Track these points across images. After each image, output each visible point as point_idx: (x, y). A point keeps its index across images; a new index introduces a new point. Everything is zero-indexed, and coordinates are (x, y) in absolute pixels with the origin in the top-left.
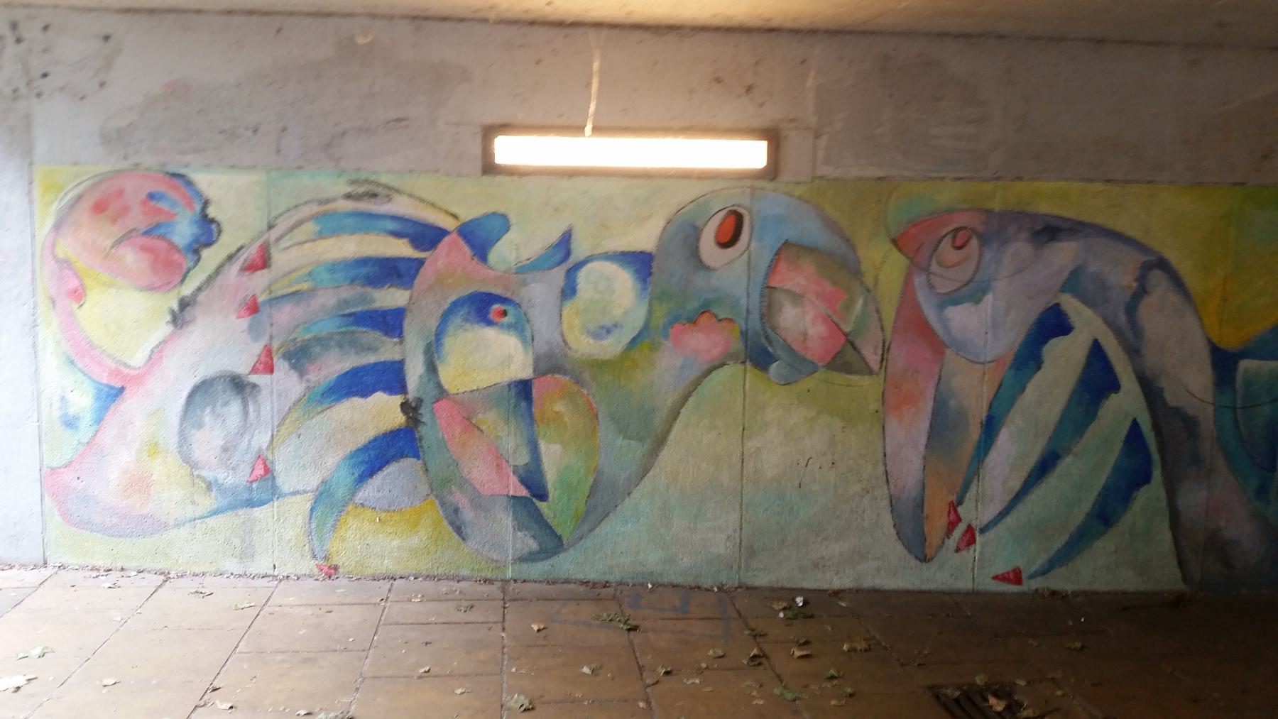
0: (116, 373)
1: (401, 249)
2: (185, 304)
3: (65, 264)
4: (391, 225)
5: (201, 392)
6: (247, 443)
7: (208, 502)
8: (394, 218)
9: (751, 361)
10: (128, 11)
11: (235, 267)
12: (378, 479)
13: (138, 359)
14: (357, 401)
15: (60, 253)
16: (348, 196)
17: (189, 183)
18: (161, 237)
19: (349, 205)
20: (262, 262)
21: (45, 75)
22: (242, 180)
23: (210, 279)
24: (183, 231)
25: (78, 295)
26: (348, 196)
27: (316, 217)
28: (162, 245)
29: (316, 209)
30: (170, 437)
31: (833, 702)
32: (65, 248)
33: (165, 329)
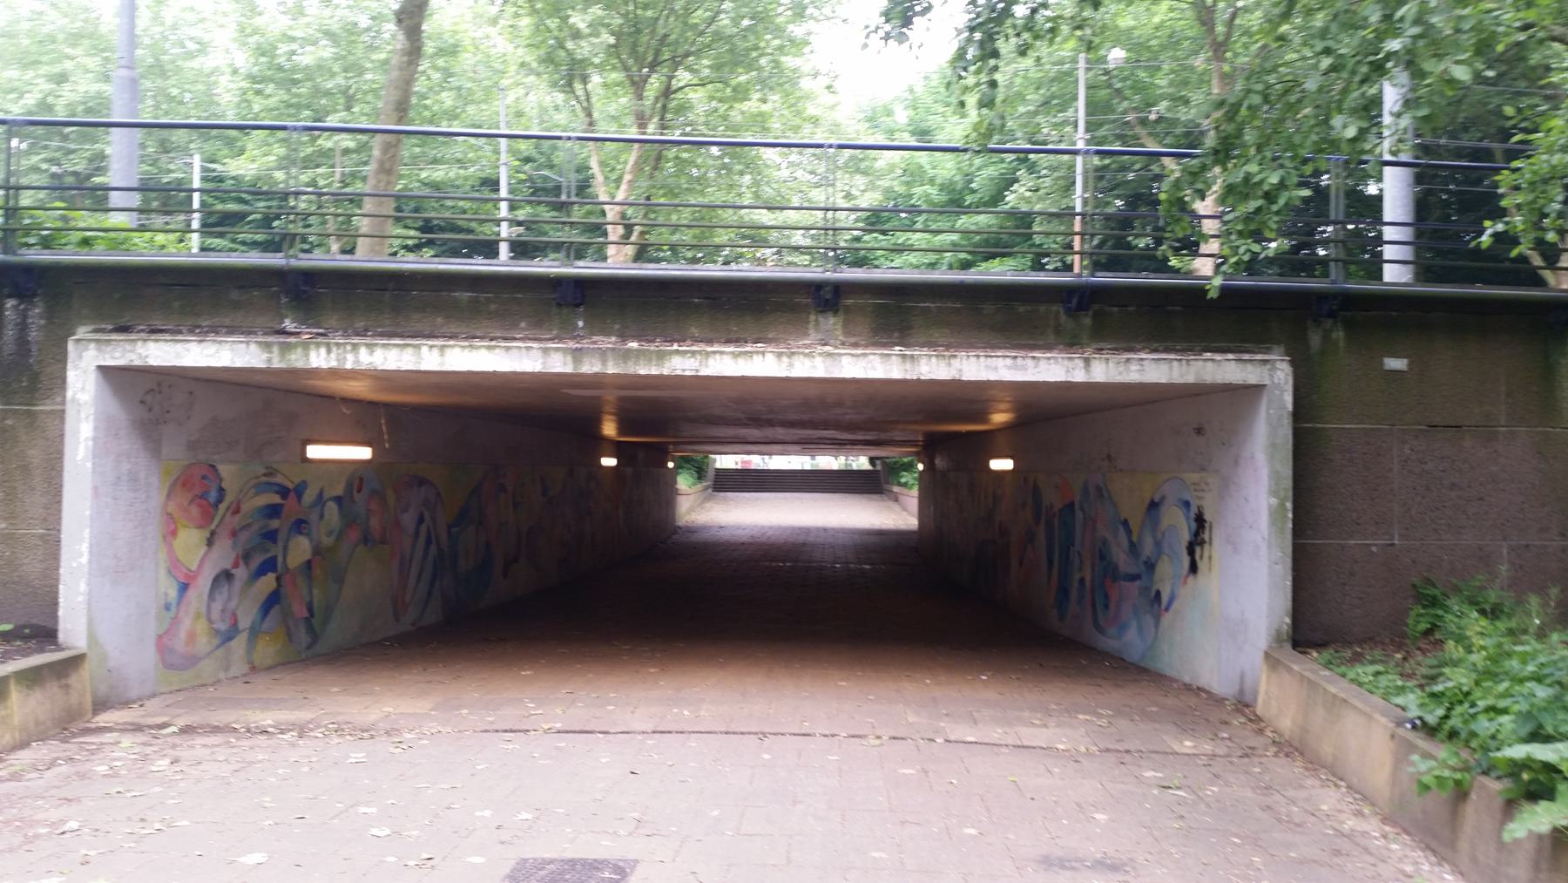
0: (186, 576)
1: (277, 499)
2: (213, 533)
3: (170, 515)
4: (276, 488)
5: (216, 581)
6: (1466, 136)
7: (216, 642)
8: (278, 485)
9: (1557, 261)
10: (808, 735)
11: (228, 514)
12: (268, 618)
13: (194, 567)
14: (263, 578)
15: (169, 511)
16: (265, 475)
17: (216, 470)
18: (206, 499)
19: (264, 479)
20: (237, 511)
21: (168, 412)
22: (233, 468)
23: (221, 520)
24: (213, 495)
25: (174, 533)
26: (265, 475)
27: (254, 486)
28: (204, 502)
29: (254, 482)
30: (204, 609)
31: (367, 781)
32: (171, 508)
33: (204, 548)
